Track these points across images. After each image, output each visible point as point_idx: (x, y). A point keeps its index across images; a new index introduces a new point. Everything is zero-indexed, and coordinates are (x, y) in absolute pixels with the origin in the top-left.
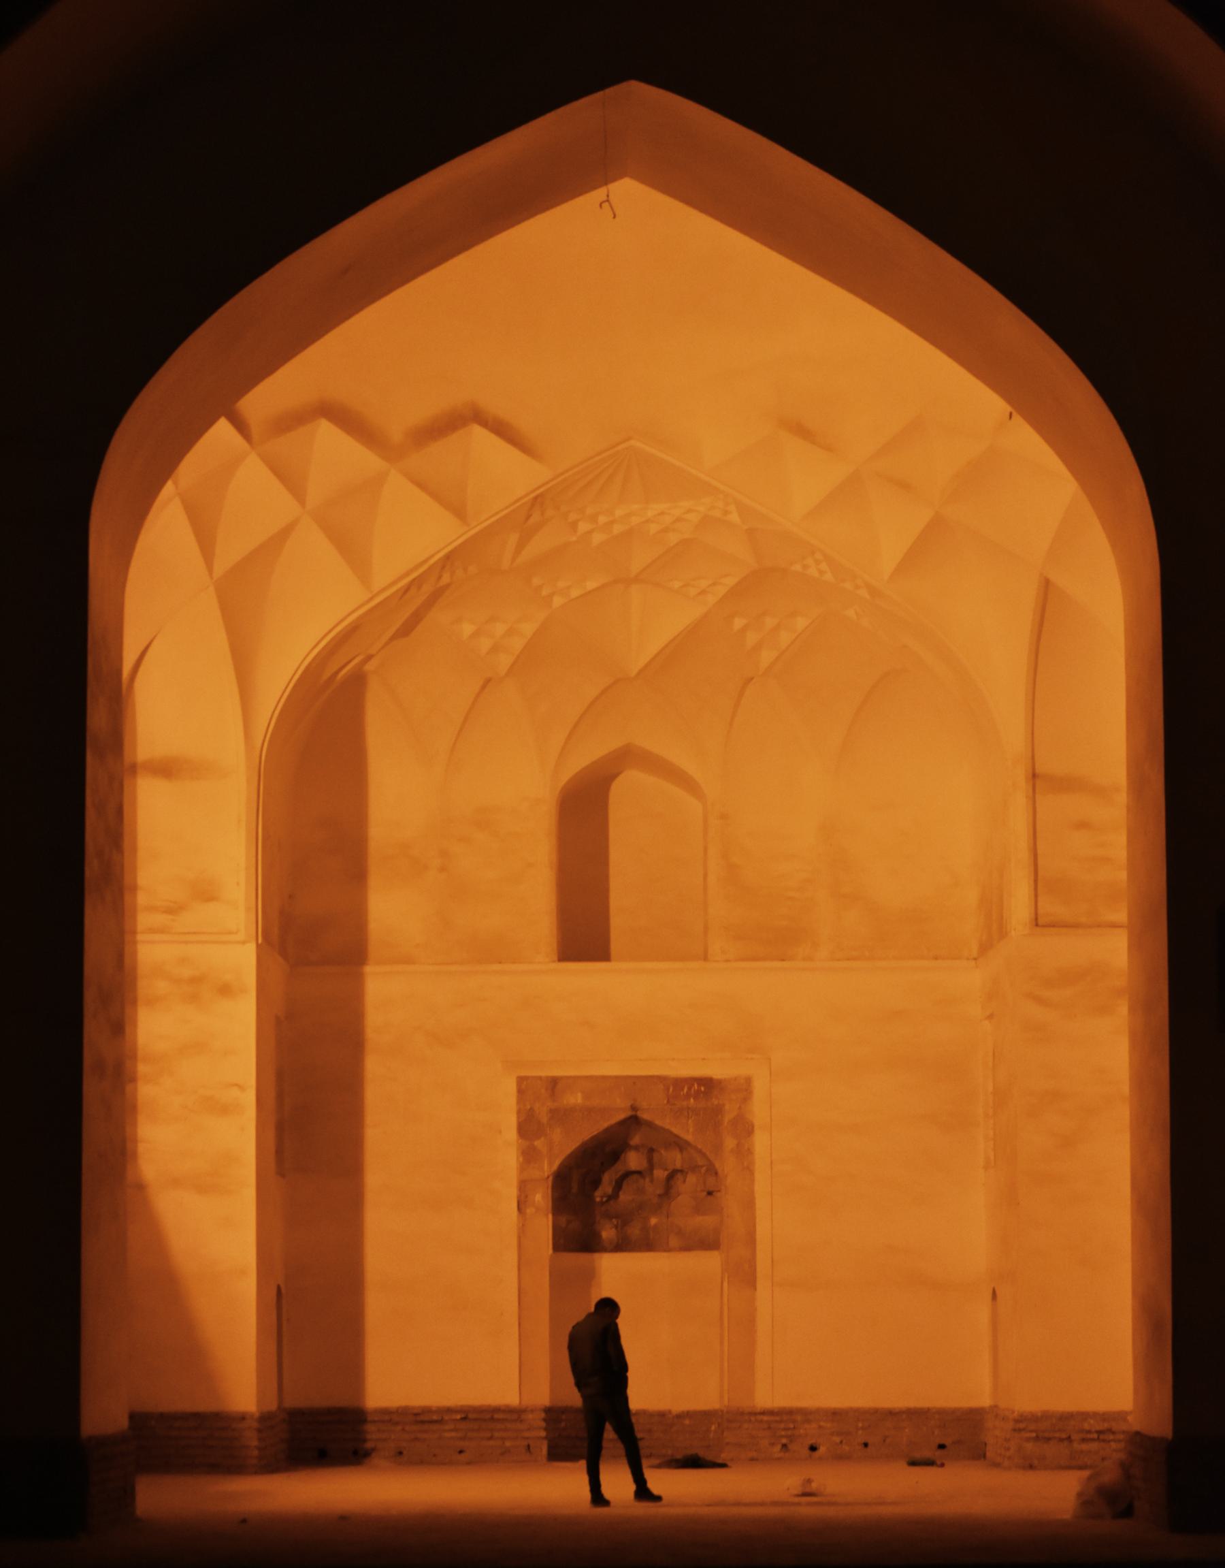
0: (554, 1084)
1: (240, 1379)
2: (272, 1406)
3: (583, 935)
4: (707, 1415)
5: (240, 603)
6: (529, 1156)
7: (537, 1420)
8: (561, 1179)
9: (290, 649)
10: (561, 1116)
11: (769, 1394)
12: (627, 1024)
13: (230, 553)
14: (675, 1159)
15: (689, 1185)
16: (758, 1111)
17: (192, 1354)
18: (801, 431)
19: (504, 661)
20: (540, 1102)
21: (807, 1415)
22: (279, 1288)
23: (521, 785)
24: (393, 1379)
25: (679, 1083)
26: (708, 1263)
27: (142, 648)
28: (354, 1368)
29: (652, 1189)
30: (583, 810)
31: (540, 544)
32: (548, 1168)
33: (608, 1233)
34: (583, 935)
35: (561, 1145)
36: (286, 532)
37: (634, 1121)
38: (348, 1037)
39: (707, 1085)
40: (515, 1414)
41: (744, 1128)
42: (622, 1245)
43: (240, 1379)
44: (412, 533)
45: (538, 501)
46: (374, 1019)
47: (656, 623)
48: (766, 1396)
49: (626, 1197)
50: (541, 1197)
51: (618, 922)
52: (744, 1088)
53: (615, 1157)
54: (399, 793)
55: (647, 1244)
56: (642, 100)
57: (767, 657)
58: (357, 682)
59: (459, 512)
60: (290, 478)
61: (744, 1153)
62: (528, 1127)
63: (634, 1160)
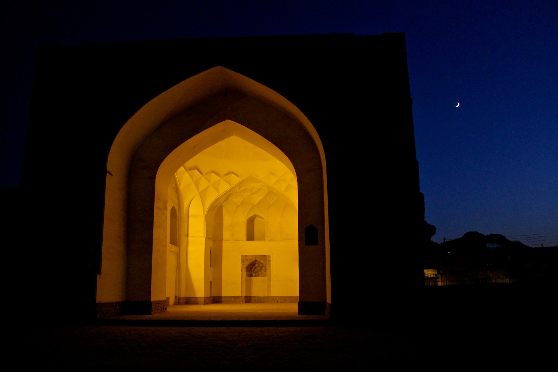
0: (246, 256)
1: (200, 291)
2: (209, 296)
3: (250, 237)
4: (266, 297)
5: (203, 195)
6: (243, 265)
7: (243, 298)
8: (247, 267)
9: (209, 201)
10: (247, 260)
11: (272, 294)
12: (255, 249)
13: (201, 189)
14: (262, 265)
15: (263, 269)
16: (271, 259)
17: (189, 284)
18: (272, 174)
19: (239, 204)
20: (244, 258)
21: (277, 297)
22: (211, 282)
23: (242, 219)
24: (225, 293)
25: (261, 256)
26: (265, 278)
27: (190, 199)
28: (221, 294)
29: (259, 269)
30: (251, 222)
31: (242, 189)
32: (245, 266)
33: (254, 274)
34: (250, 237)
35: (247, 263)
36: (208, 187)
37: (256, 260)
38: (220, 250)
39: (265, 256)
40: (241, 297)
41: (269, 261)
42: (255, 276)
43: (200, 291)
44: (224, 187)
45: (240, 183)
46: (224, 248)
47: (257, 199)
48: (272, 295)
49: (256, 270)
50: (244, 270)
51: (255, 236)
52: (269, 256)
53: (254, 265)
54: (227, 220)
55: (259, 276)
56: (229, 123)
57: (271, 203)
58: (221, 207)
59: (230, 184)
60: (209, 180)
61: (269, 264)
62: (243, 261)
63: (257, 265)
